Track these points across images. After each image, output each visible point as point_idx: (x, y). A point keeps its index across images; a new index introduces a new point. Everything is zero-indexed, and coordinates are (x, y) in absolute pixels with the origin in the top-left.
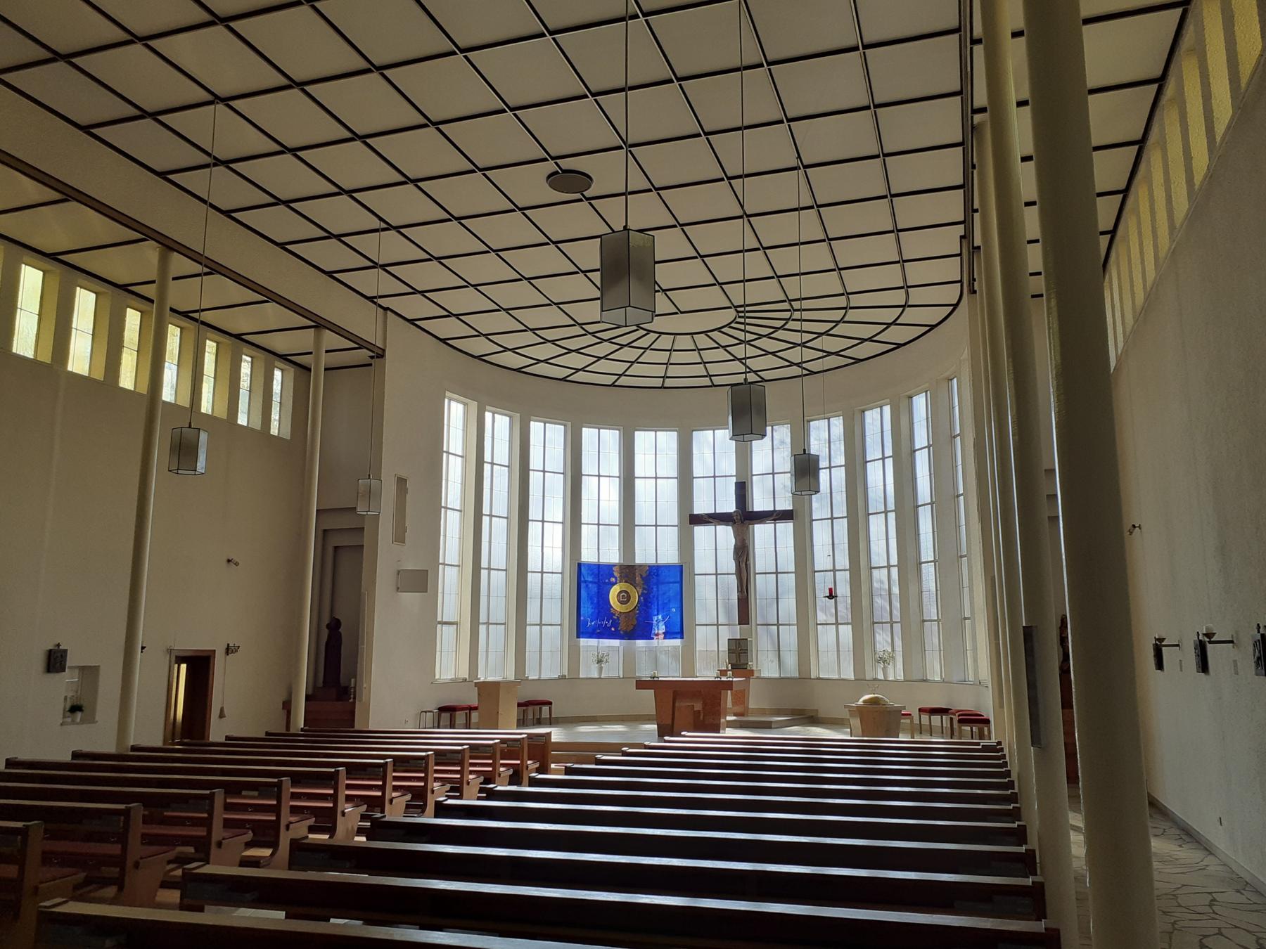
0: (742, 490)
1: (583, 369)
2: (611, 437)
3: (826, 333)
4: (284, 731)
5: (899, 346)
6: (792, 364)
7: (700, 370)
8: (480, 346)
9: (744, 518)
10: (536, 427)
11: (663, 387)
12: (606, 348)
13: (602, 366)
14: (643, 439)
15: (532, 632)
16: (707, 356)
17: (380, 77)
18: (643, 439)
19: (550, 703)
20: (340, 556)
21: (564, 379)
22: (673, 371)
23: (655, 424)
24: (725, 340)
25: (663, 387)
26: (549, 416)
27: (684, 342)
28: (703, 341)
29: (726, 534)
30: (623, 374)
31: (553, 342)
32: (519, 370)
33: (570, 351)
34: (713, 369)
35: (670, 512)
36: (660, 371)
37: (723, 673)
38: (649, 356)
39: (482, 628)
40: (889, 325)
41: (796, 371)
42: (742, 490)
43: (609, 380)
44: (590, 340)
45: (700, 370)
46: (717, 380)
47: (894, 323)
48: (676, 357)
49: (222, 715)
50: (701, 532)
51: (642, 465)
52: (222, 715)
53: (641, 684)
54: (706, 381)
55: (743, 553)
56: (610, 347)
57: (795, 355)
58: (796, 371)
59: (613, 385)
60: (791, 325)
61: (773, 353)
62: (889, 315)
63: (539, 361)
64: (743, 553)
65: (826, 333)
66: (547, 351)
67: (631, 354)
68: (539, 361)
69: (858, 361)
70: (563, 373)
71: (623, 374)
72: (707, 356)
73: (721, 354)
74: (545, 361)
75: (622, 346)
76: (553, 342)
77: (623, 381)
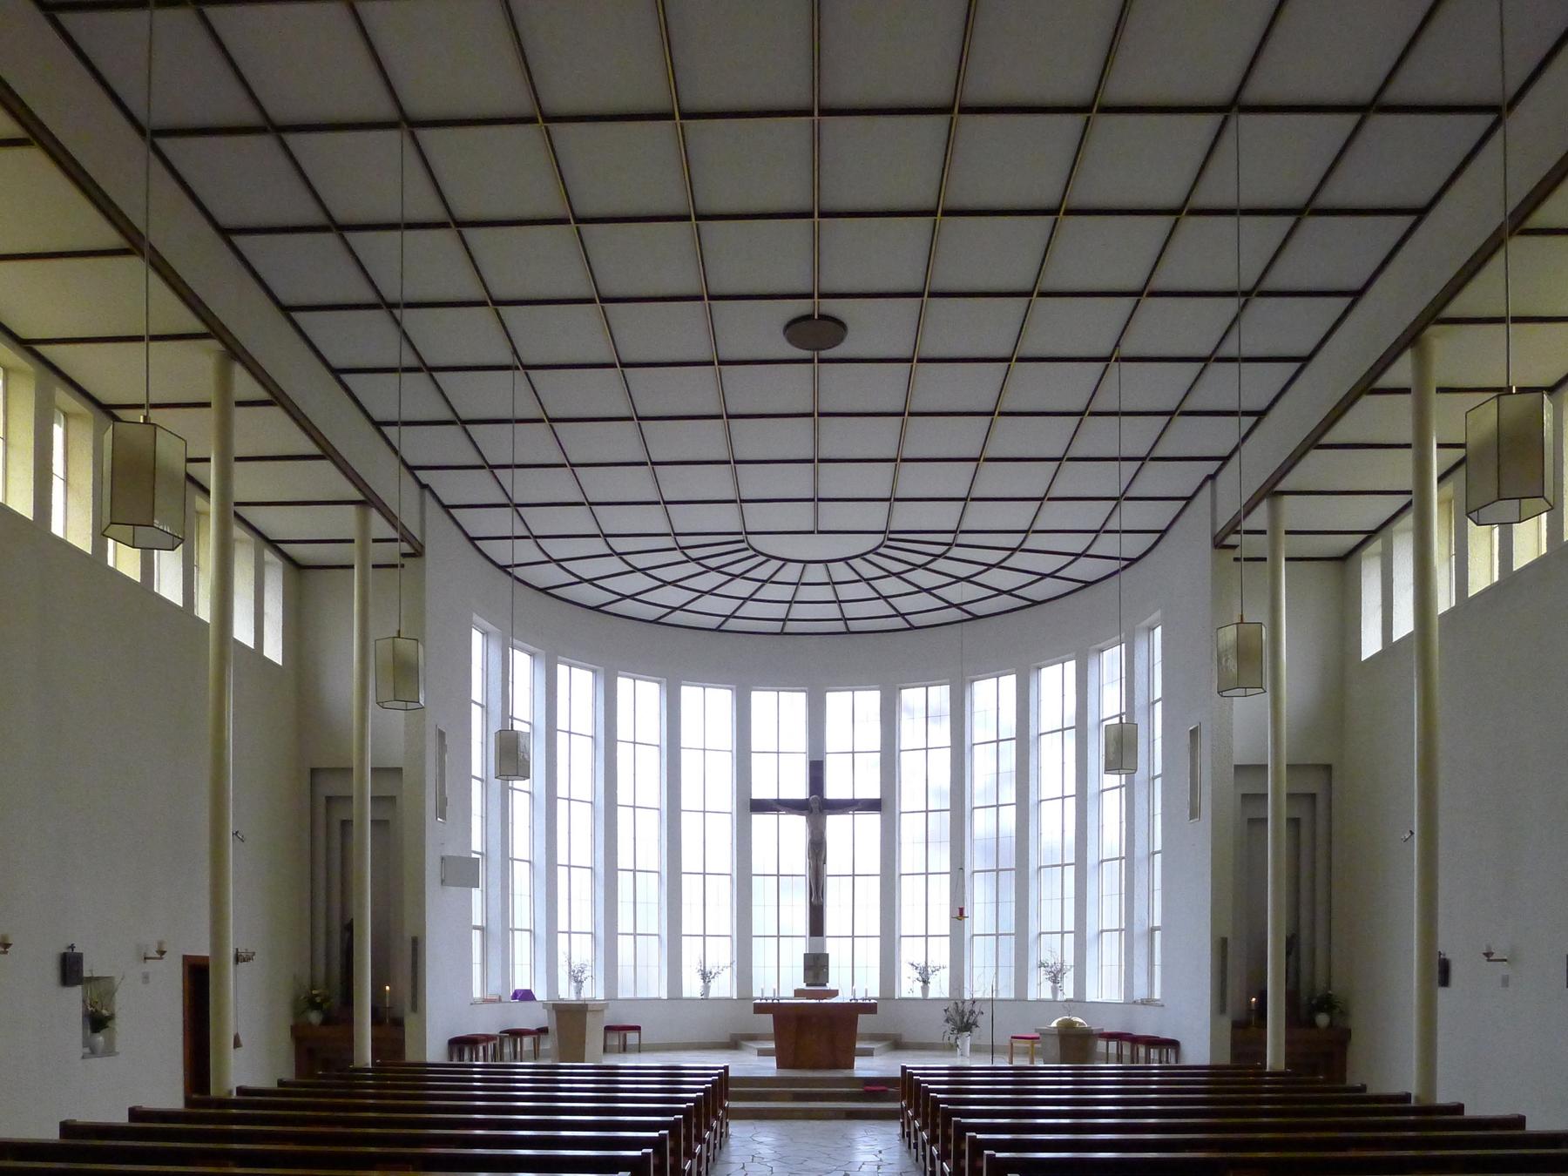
0: (816, 771)
1: (680, 608)
2: (869, 701)
3: (998, 565)
4: (446, 1062)
5: (1087, 584)
6: (951, 605)
7: (833, 611)
8: (548, 575)
9: (816, 806)
10: (624, 684)
11: (782, 633)
12: (713, 579)
13: (707, 604)
14: (837, 702)
15: (624, 945)
16: (845, 592)
17: (1193, 219)
18: (837, 702)
19: (638, 1029)
20: (352, 848)
21: (656, 622)
22: (798, 611)
23: (853, 682)
24: (868, 571)
25: (782, 633)
26: (641, 669)
27: (816, 573)
28: (841, 572)
29: (796, 827)
30: (732, 616)
31: (643, 570)
32: (596, 609)
33: (665, 583)
34: (851, 610)
35: (724, 797)
36: (779, 611)
37: (798, 993)
38: (769, 592)
39: (1070, 925)
40: (1077, 556)
41: (954, 614)
42: (816, 771)
43: (714, 622)
44: (694, 568)
45: (833, 611)
46: (854, 625)
47: (1084, 554)
48: (805, 593)
49: (237, 1044)
50: (762, 823)
51: (761, 737)
52: (237, 1044)
53: (760, 1009)
54: (840, 627)
55: (817, 848)
56: (719, 578)
57: (956, 593)
58: (954, 614)
59: (718, 630)
60: (955, 552)
61: (928, 591)
62: (1077, 543)
63: (624, 597)
64: (817, 848)
65: (998, 565)
66: (637, 583)
67: (742, 588)
68: (624, 597)
69: (1035, 603)
70: (657, 612)
71: (732, 616)
72: (845, 592)
73: (862, 590)
74: (632, 597)
75: (735, 576)
76: (643, 570)
77: (732, 624)
